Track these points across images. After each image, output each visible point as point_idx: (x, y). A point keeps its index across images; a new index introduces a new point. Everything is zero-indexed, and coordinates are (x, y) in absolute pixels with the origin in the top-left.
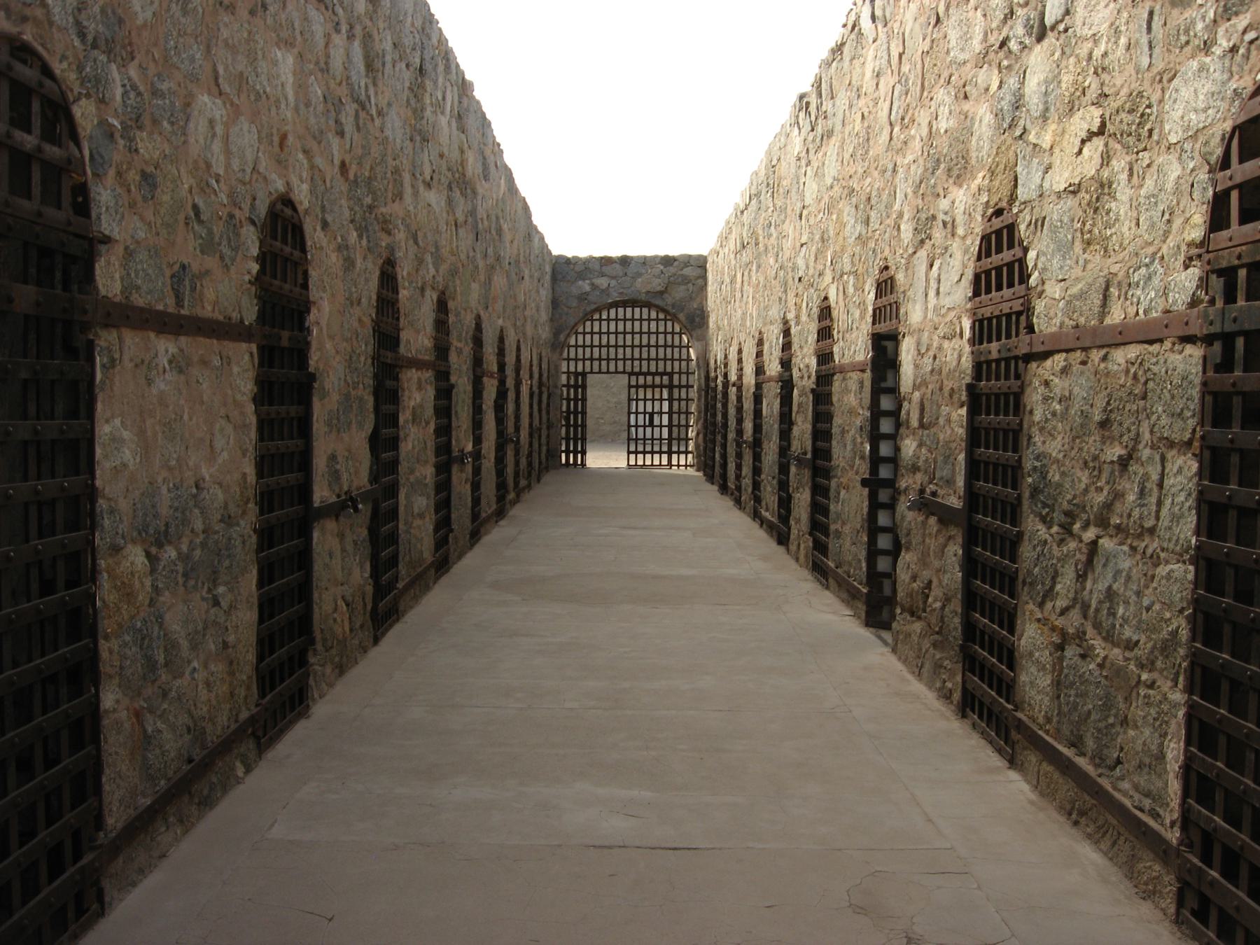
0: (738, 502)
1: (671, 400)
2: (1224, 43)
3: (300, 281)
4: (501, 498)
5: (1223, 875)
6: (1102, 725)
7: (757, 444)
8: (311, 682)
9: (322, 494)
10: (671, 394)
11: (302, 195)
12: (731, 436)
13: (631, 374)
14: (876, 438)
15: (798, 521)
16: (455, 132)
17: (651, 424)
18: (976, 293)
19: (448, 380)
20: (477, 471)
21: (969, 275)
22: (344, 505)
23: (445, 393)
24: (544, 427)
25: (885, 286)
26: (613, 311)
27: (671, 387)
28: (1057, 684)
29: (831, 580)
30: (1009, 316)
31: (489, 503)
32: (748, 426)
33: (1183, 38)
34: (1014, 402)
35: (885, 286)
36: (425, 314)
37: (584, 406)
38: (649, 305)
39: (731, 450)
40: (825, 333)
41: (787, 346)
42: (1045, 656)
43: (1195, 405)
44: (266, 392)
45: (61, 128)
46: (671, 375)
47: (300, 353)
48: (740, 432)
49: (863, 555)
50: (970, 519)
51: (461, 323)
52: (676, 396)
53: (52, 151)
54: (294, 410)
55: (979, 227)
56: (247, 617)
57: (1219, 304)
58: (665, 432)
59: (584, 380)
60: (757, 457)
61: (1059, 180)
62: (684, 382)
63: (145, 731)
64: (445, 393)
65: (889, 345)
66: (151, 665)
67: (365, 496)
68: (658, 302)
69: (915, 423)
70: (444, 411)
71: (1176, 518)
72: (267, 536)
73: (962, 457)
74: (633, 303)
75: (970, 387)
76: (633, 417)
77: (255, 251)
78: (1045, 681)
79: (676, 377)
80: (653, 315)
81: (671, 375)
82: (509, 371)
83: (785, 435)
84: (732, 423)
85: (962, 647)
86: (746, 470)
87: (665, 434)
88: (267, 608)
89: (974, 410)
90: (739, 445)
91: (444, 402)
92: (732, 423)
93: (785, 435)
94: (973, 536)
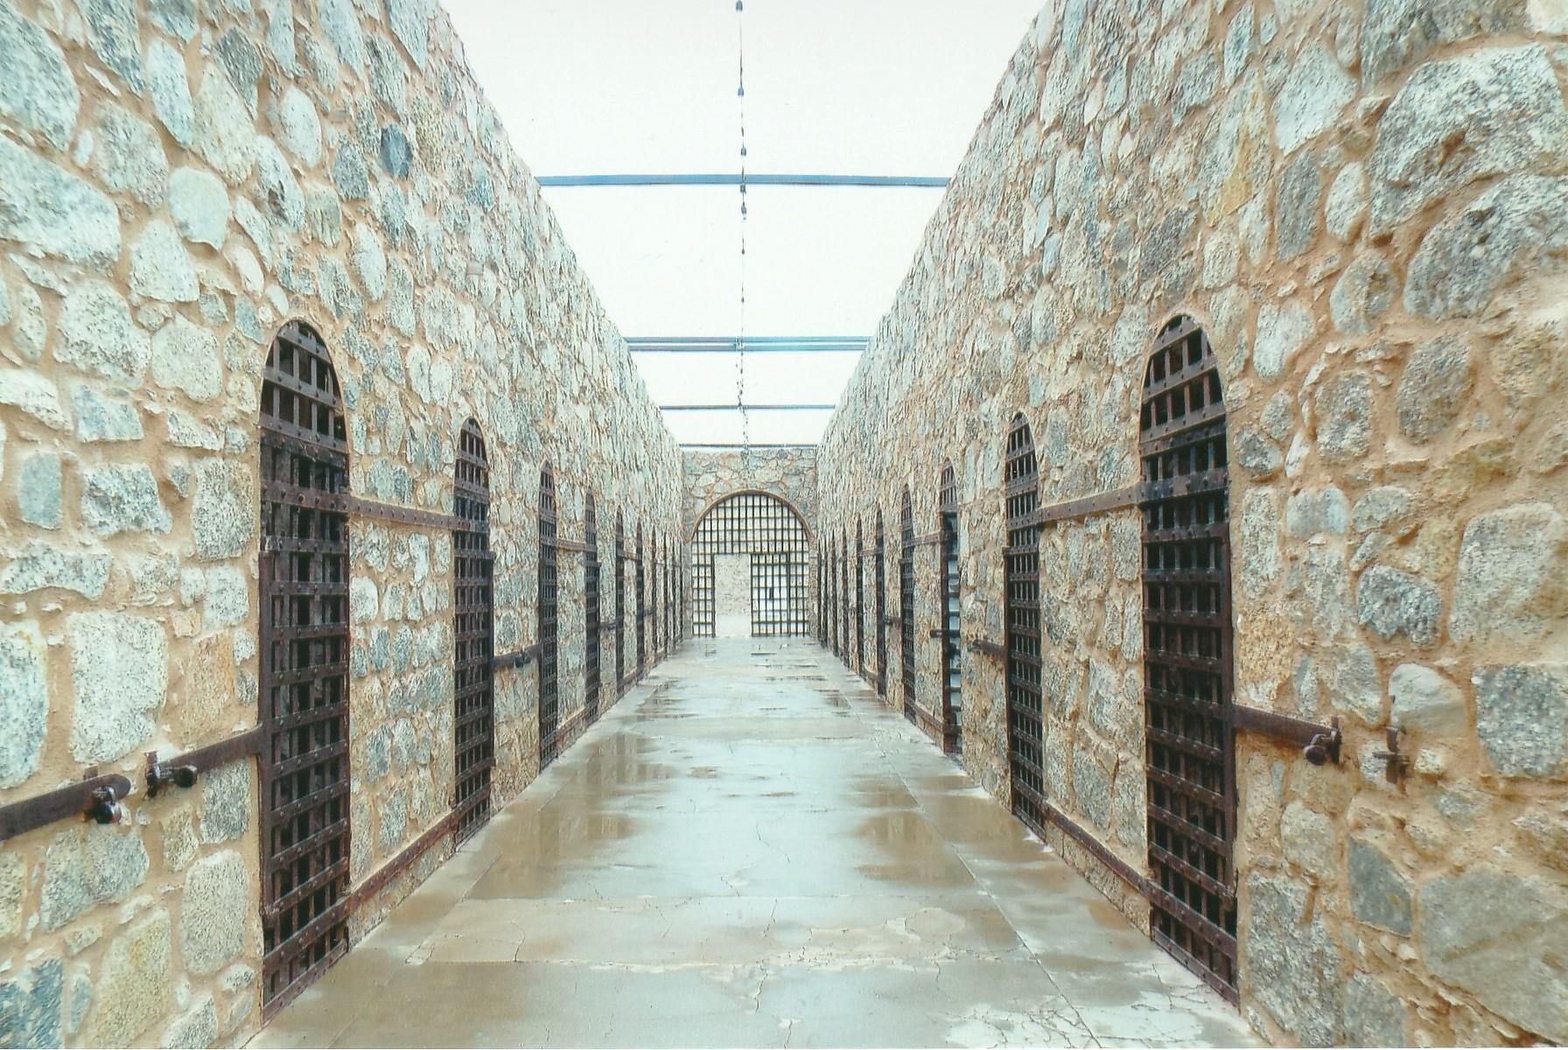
0: (847, 661)
1: (789, 576)
2: (1145, 297)
3: (482, 481)
4: (641, 662)
5: (1176, 895)
6: (1099, 798)
7: (859, 608)
8: (492, 796)
9: (498, 651)
10: (788, 571)
11: (483, 416)
12: (840, 604)
13: (753, 554)
14: (945, 599)
15: (893, 671)
16: (596, 353)
17: (772, 598)
18: (1007, 478)
19: (595, 559)
20: (620, 637)
21: (1003, 465)
22: (518, 661)
23: (594, 571)
24: (678, 601)
25: (948, 474)
26: (743, 500)
27: (788, 565)
28: (1070, 771)
29: (917, 717)
30: (1022, 496)
31: (630, 670)
32: (853, 596)
33: (1122, 292)
34: (1033, 560)
35: (948, 474)
36: (578, 509)
37: (713, 584)
38: (760, 494)
39: (840, 616)
40: (906, 515)
41: (880, 526)
42: (1060, 753)
43: (1139, 554)
44: (460, 566)
45: (328, 379)
46: (788, 554)
47: (482, 539)
48: (846, 601)
49: (940, 693)
50: (1009, 656)
51: (606, 516)
52: (793, 573)
53: (310, 390)
54: (481, 581)
55: (1007, 427)
56: (446, 737)
57: (1149, 481)
58: (784, 605)
59: (712, 560)
60: (860, 621)
61: (1055, 393)
62: (799, 560)
63: (377, 813)
64: (594, 571)
65: (953, 521)
66: (382, 765)
67: (534, 651)
68: (775, 492)
69: (971, 582)
70: (593, 586)
71: (1133, 636)
72: (461, 676)
73: (1002, 607)
74: (754, 494)
75: (1005, 551)
76: (755, 592)
77: (452, 460)
78: (1062, 773)
79: (793, 556)
80: (771, 503)
81: (788, 554)
82: (647, 553)
83: (881, 600)
84: (840, 592)
85: (1010, 756)
86: (852, 633)
87: (784, 606)
88: (461, 733)
89: (1009, 568)
90: (846, 613)
91: (593, 593)
92: (840, 592)
93: (881, 600)
94: (1010, 670)
